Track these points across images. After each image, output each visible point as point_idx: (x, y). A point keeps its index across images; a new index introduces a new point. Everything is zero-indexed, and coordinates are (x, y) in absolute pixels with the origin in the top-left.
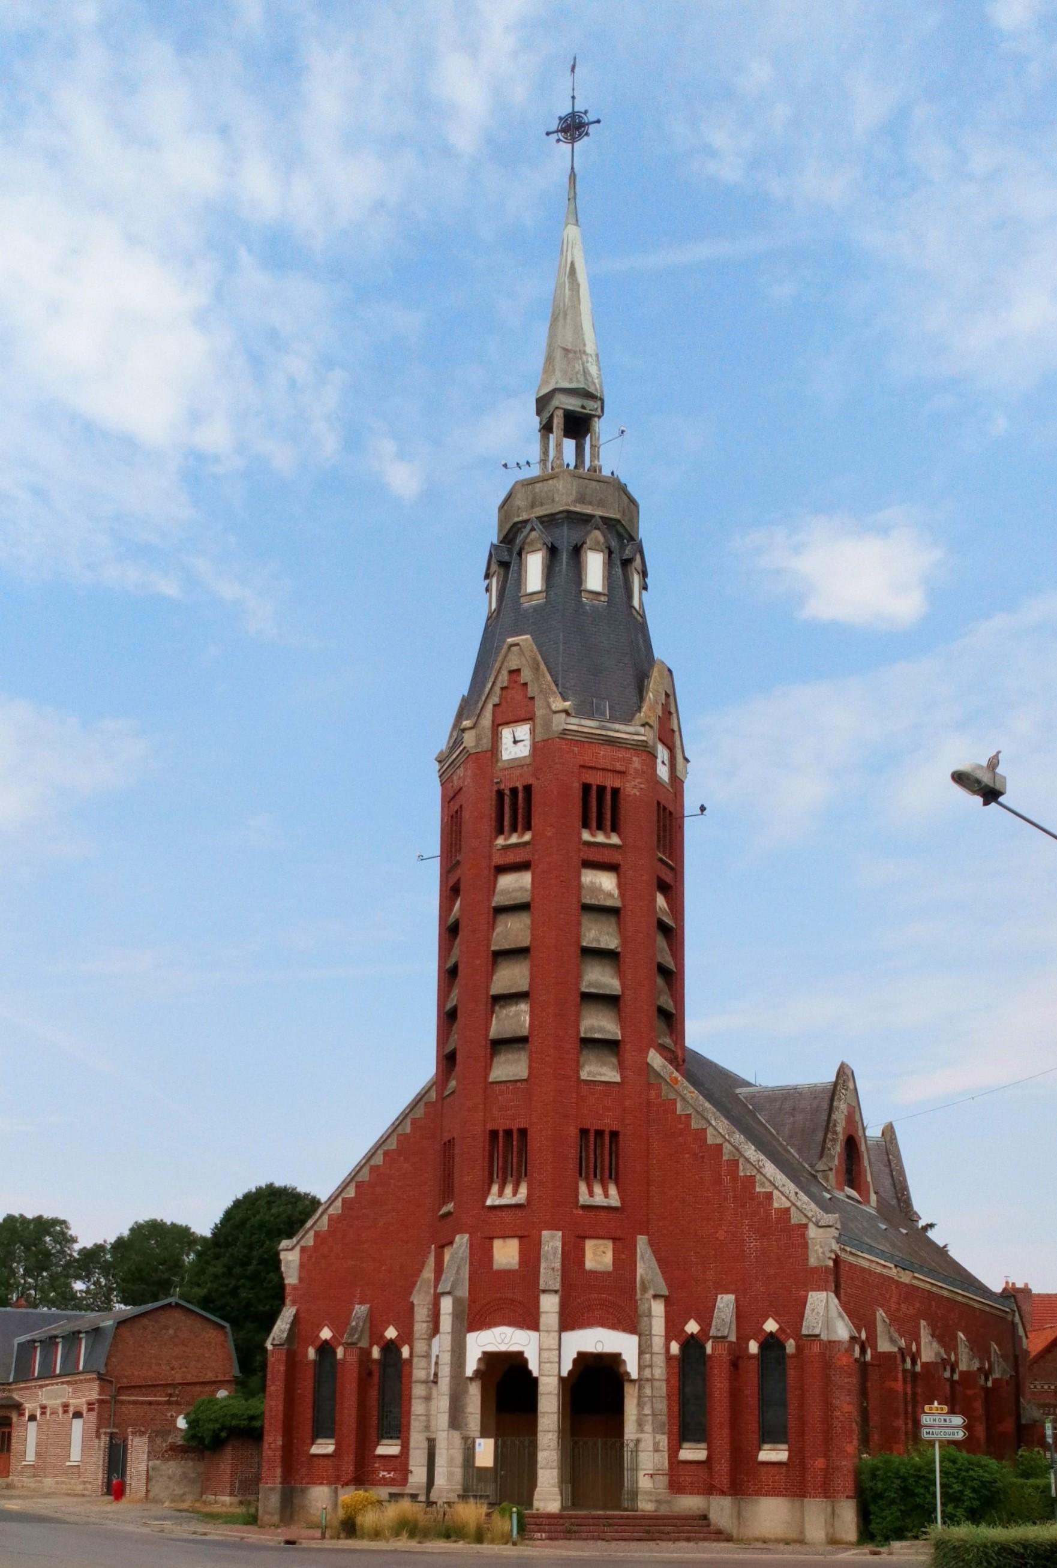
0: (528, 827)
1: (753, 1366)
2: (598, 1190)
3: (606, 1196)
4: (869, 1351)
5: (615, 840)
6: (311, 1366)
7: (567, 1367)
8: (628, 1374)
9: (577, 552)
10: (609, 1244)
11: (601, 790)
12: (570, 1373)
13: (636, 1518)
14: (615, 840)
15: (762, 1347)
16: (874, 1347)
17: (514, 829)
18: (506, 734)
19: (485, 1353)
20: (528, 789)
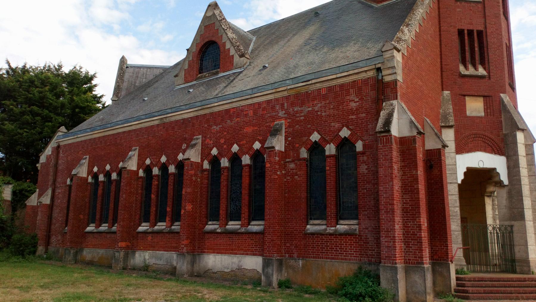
1: (246, 173)
3: (476, 69)
5: (481, 71)
7: (460, 177)
10: (481, 99)
12: (463, 181)
15: (338, 148)
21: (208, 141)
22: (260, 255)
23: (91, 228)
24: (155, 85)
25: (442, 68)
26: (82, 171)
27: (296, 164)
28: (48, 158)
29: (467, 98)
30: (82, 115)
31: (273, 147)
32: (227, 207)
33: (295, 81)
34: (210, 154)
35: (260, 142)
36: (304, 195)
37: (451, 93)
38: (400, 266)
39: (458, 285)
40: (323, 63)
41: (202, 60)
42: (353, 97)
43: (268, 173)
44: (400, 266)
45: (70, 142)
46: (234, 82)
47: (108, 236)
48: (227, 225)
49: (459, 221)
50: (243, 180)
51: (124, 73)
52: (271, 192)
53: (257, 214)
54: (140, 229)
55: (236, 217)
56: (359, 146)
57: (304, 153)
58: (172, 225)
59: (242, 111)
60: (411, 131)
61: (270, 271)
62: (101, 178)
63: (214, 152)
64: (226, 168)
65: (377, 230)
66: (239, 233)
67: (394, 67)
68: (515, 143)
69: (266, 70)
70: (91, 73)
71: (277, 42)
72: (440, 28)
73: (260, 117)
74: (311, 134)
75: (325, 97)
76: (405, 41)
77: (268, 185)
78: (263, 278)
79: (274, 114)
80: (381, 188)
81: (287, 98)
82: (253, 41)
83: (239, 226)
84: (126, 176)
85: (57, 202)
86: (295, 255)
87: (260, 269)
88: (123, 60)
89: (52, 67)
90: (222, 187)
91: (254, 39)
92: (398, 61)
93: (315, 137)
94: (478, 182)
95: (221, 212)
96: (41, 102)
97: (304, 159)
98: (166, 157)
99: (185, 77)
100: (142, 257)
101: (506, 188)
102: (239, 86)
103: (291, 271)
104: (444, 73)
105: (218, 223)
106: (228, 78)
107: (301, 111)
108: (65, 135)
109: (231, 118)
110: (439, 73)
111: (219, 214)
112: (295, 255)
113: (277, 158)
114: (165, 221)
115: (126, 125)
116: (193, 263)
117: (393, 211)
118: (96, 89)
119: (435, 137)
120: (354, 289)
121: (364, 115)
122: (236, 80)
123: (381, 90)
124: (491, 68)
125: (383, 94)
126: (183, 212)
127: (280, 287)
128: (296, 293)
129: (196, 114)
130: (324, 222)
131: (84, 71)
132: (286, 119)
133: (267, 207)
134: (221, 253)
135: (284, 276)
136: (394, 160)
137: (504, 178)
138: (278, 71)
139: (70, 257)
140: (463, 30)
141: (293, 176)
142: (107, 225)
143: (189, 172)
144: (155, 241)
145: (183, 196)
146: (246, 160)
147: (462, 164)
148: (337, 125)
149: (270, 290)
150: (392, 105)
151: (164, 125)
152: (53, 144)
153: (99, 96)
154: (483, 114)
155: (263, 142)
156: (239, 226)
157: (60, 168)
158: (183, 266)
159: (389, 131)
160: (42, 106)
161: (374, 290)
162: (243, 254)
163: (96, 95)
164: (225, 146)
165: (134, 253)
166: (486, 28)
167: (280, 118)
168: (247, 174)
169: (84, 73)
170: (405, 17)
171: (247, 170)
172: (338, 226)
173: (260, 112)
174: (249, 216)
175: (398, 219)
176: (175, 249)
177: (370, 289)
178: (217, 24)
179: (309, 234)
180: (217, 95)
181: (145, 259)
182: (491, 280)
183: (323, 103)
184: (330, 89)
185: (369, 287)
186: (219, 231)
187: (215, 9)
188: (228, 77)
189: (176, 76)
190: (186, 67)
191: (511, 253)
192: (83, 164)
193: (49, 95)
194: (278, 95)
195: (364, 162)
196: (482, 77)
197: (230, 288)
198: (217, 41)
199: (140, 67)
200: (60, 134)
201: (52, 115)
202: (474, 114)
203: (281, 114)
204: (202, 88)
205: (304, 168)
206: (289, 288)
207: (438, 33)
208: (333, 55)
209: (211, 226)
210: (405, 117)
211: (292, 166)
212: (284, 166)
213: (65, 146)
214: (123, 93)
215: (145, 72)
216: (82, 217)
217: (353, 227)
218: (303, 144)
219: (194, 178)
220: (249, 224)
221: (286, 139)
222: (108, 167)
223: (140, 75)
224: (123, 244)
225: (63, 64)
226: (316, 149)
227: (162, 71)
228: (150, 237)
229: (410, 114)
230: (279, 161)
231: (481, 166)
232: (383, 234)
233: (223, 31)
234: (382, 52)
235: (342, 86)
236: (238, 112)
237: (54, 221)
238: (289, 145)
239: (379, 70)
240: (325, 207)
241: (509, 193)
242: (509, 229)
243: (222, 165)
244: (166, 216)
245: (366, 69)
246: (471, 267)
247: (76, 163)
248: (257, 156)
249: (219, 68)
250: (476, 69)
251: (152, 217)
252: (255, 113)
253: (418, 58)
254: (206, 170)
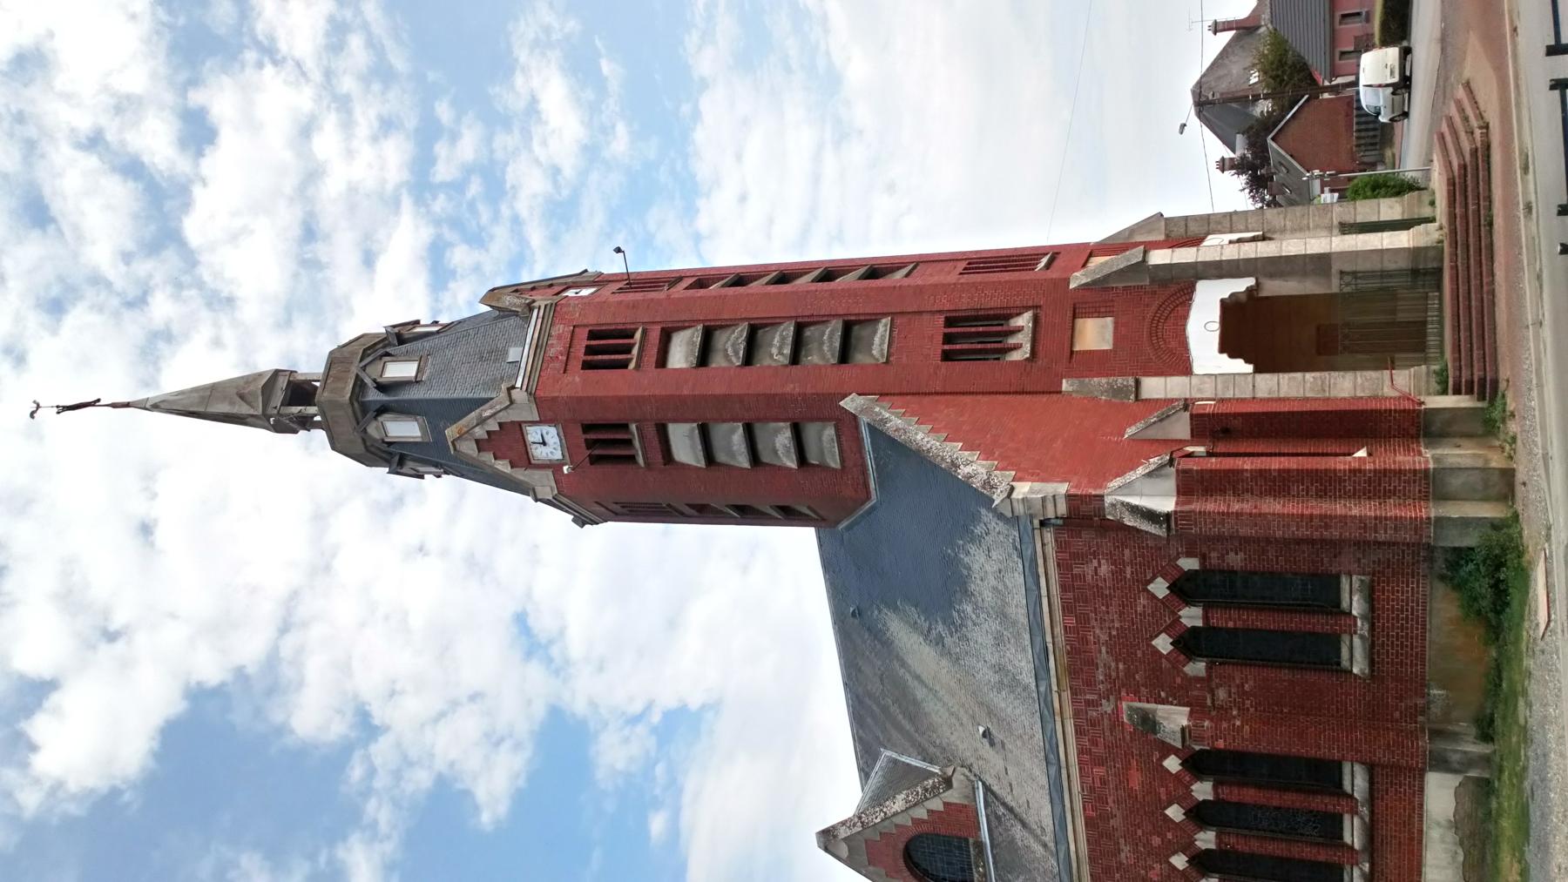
0: (624, 427)
1: (1233, 794)
2: (1012, 341)
5: (1024, 321)
7: (1241, 366)
8: (1249, 290)
9: (383, 387)
10: (1079, 322)
11: (590, 350)
14: (638, 335)
15: (1189, 600)
17: (629, 443)
18: (540, 453)
19: (1222, 351)
20: (587, 428)
22: (1422, 777)
29: (1077, 348)
31: (1183, 729)
32: (1312, 844)
35: (1164, 756)
36: (1285, 674)
37: (1068, 376)
38: (1433, 511)
39: (1470, 391)
40: (1002, 615)
43: (1238, 745)
44: (1433, 511)
46: (1013, 804)
48: (1352, 848)
52: (1278, 741)
53: (1326, 776)
55: (1331, 828)
56: (1189, 564)
57: (1197, 668)
59: (1092, 789)
60: (1167, 476)
65: (1361, 545)
66: (1372, 820)
67: (1044, 499)
69: (994, 732)
71: (915, 703)
74: (1156, 652)
75: (1083, 621)
76: (989, 474)
77: (1263, 747)
78: (1473, 774)
79: (1106, 721)
80: (1279, 534)
81: (1074, 692)
82: (895, 755)
83: (1356, 820)
86: (1420, 702)
91: (889, 753)
92: (1032, 491)
93: (1163, 644)
94: (1244, 329)
95: (1322, 858)
97: (1209, 668)
101: (1262, 280)
102: (1030, 790)
105: (1348, 868)
106: (998, 818)
110: (1028, 398)
117: (1322, 517)
119: (1165, 423)
120: (1484, 597)
121: (1127, 552)
122: (1008, 799)
123: (1083, 521)
124: (1018, 303)
127: (1492, 740)
128: (1501, 706)
130: (1345, 638)
133: (1313, 753)
135: (1466, 727)
136: (1223, 508)
137: (1241, 285)
140: (944, 352)
141: (1243, 694)
146: (1203, 790)
149: (1497, 759)
150: (1113, 505)
154: (1109, 320)
155: (1167, 750)
156: (1356, 820)
159: (1168, 516)
161: (1484, 562)
162: (1421, 816)
164: (1169, 836)
167: (1117, 710)
170: (936, 467)
171: (1226, 790)
172: (1354, 612)
173: (1099, 750)
174: (1331, 794)
175: (1339, 508)
177: (1482, 569)
178: (869, 834)
179: (1372, 671)
180: (1045, 846)
182: (1457, 328)
183: (1093, 623)
185: (1478, 570)
186: (1366, 867)
187: (835, 837)
188: (994, 820)
194: (1068, 711)
197: (1496, 844)
202: (1109, 336)
203: (1107, 707)
205: (1229, 669)
206: (1492, 721)
210: (1138, 484)
211: (1222, 694)
212: (1222, 712)
217: (1356, 585)
218: (1176, 667)
220: (1351, 796)
221: (1163, 702)
226: (1189, 643)
230: (1211, 720)
231: (1217, 326)
232: (1370, 536)
233: (886, 823)
235: (1064, 588)
236: (1094, 797)
238: (1178, 696)
239: (1043, 524)
242: (1348, 279)
243: (1213, 846)
245: (1039, 546)
248: (1197, 765)
249: (966, 840)
250: (1019, 330)
252: (1100, 762)
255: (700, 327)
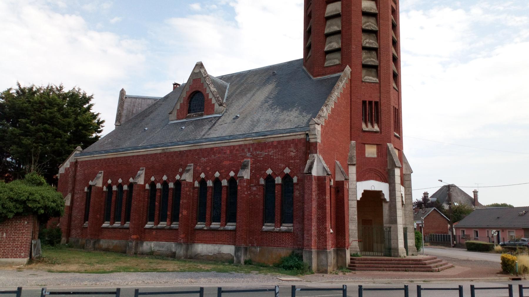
2: (369, 124)
4: (332, 180)
5: (376, 128)
6: (125, 193)
7: (359, 196)
8: (385, 200)
10: (375, 146)
12: (361, 198)
13: (400, 260)
15: (283, 179)
16: (334, 178)
19: (365, 191)
21: (198, 168)
22: (233, 244)
23: (106, 225)
24: (151, 116)
25: (351, 126)
26: (99, 182)
27: (257, 188)
28: (67, 170)
29: (366, 146)
30: (84, 132)
31: (243, 177)
32: (211, 212)
33: (258, 134)
34: (199, 176)
37: (356, 143)
38: (314, 250)
39: (351, 263)
40: (276, 122)
41: (190, 103)
42: (292, 149)
43: (239, 193)
44: (314, 250)
45: (87, 159)
46: (216, 125)
47: (121, 231)
49: (357, 224)
50: (223, 196)
51: (123, 103)
52: (241, 205)
53: (232, 217)
54: (147, 226)
55: (216, 219)
56: (295, 180)
57: (262, 181)
58: (171, 224)
59: (222, 150)
60: (324, 173)
61: (239, 254)
62: (115, 188)
63: (203, 175)
64: (211, 187)
65: (303, 230)
66: (219, 230)
67: (315, 135)
68: (394, 175)
69: (238, 119)
70: (88, 95)
71: (245, 94)
72: (351, 99)
73: (234, 155)
74: (267, 169)
75: (276, 147)
76: (323, 117)
77: (239, 200)
80: (306, 206)
81: (252, 145)
82: (228, 88)
84: (137, 189)
85: (76, 204)
86: (255, 245)
87: (233, 253)
88: (122, 92)
89: (54, 87)
90: (208, 199)
91: (228, 86)
92: (318, 131)
93: (269, 172)
94: (372, 199)
95: (207, 216)
96: (52, 121)
97: (262, 185)
98: (167, 176)
99: (178, 115)
100: (147, 246)
103: (252, 254)
104: (353, 130)
106: (211, 121)
107: (261, 154)
108: (82, 154)
109: (214, 153)
110: (349, 130)
111: (205, 218)
112: (255, 245)
113: (245, 184)
114: (166, 221)
115: (135, 151)
116: (187, 249)
117: (311, 219)
118: (93, 107)
121: (298, 161)
123: (308, 147)
125: (309, 149)
126: (180, 215)
129: (189, 148)
130: (273, 224)
131: (82, 92)
132: (251, 158)
133: (238, 214)
134: (207, 243)
135: (248, 257)
136: (313, 190)
137: (387, 197)
138: (247, 122)
139: (91, 246)
142: (120, 222)
143: (185, 189)
144: (158, 235)
145: (181, 205)
146: (225, 183)
147: (360, 188)
148: (283, 166)
150: (314, 157)
151: (165, 154)
152: (71, 159)
153: (95, 114)
154: (376, 156)
155: (236, 172)
157: (78, 178)
158: (180, 251)
159: (311, 173)
160: (52, 124)
162: (221, 244)
163: (93, 113)
164: (210, 173)
165: (142, 243)
166: (380, 100)
168: (225, 192)
169: (82, 93)
170: (326, 99)
171: (225, 189)
172: (281, 227)
173: (235, 152)
175: (314, 224)
176: (175, 240)
178: (202, 79)
179: (264, 232)
180: (204, 135)
181: (151, 247)
182: (371, 260)
183: (275, 150)
184: (279, 142)
189: (170, 113)
190: (178, 108)
191: (389, 243)
192: (99, 177)
193: (58, 115)
195: (297, 189)
196: (376, 132)
198: (202, 91)
199: (136, 98)
200: (78, 152)
201: (61, 132)
202: (370, 156)
204: (191, 127)
207: (349, 104)
208: (282, 117)
209: (199, 226)
210: (320, 164)
211: (255, 189)
212: (249, 189)
213: (82, 162)
214: (123, 119)
215: (140, 102)
216: (98, 216)
217: (290, 228)
219: (188, 193)
220: (226, 225)
221: (251, 171)
222: (120, 181)
223: (136, 105)
224: (135, 237)
225: (64, 86)
226: (270, 179)
227: (154, 102)
228: (154, 232)
229: (323, 162)
231: (373, 189)
234: (308, 125)
235: (286, 141)
236: (220, 150)
237: (73, 219)
238: (253, 175)
239: (307, 134)
240: (274, 216)
241: (390, 206)
242: (388, 229)
243: (208, 185)
244: (167, 218)
245: (300, 133)
246: (364, 253)
247: (93, 176)
248: (232, 181)
249: (203, 111)
250: (373, 127)
251: (156, 218)
252: (231, 152)
253: (333, 124)
254: (196, 188)
255: (377, 12)
